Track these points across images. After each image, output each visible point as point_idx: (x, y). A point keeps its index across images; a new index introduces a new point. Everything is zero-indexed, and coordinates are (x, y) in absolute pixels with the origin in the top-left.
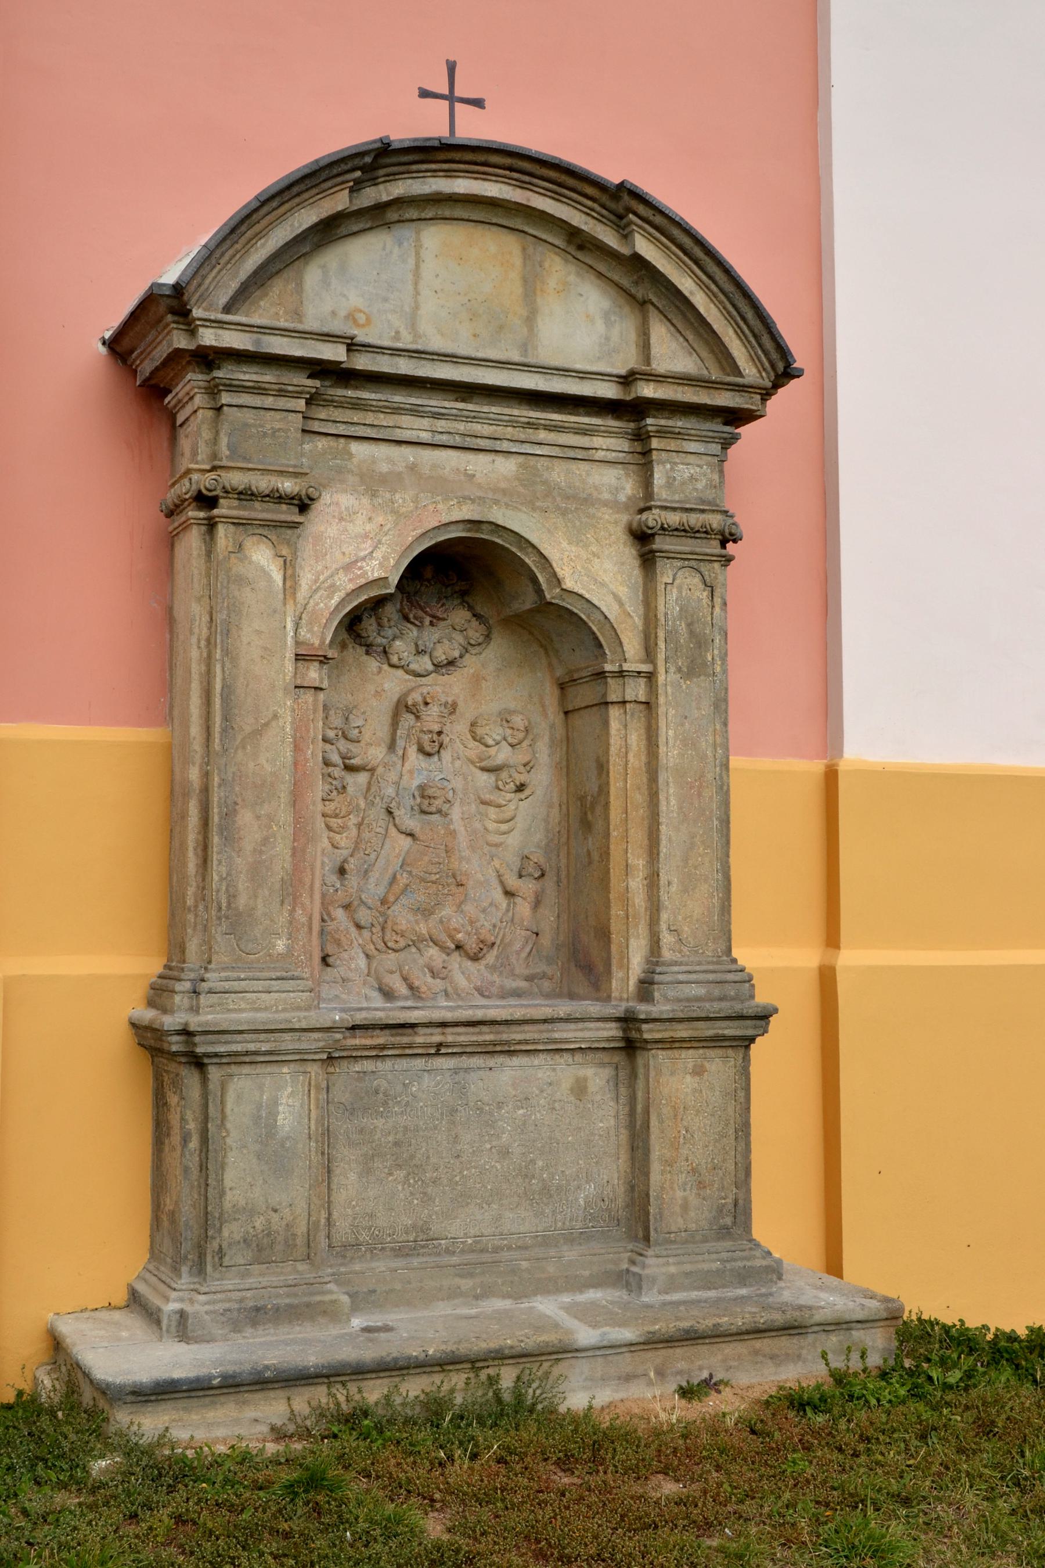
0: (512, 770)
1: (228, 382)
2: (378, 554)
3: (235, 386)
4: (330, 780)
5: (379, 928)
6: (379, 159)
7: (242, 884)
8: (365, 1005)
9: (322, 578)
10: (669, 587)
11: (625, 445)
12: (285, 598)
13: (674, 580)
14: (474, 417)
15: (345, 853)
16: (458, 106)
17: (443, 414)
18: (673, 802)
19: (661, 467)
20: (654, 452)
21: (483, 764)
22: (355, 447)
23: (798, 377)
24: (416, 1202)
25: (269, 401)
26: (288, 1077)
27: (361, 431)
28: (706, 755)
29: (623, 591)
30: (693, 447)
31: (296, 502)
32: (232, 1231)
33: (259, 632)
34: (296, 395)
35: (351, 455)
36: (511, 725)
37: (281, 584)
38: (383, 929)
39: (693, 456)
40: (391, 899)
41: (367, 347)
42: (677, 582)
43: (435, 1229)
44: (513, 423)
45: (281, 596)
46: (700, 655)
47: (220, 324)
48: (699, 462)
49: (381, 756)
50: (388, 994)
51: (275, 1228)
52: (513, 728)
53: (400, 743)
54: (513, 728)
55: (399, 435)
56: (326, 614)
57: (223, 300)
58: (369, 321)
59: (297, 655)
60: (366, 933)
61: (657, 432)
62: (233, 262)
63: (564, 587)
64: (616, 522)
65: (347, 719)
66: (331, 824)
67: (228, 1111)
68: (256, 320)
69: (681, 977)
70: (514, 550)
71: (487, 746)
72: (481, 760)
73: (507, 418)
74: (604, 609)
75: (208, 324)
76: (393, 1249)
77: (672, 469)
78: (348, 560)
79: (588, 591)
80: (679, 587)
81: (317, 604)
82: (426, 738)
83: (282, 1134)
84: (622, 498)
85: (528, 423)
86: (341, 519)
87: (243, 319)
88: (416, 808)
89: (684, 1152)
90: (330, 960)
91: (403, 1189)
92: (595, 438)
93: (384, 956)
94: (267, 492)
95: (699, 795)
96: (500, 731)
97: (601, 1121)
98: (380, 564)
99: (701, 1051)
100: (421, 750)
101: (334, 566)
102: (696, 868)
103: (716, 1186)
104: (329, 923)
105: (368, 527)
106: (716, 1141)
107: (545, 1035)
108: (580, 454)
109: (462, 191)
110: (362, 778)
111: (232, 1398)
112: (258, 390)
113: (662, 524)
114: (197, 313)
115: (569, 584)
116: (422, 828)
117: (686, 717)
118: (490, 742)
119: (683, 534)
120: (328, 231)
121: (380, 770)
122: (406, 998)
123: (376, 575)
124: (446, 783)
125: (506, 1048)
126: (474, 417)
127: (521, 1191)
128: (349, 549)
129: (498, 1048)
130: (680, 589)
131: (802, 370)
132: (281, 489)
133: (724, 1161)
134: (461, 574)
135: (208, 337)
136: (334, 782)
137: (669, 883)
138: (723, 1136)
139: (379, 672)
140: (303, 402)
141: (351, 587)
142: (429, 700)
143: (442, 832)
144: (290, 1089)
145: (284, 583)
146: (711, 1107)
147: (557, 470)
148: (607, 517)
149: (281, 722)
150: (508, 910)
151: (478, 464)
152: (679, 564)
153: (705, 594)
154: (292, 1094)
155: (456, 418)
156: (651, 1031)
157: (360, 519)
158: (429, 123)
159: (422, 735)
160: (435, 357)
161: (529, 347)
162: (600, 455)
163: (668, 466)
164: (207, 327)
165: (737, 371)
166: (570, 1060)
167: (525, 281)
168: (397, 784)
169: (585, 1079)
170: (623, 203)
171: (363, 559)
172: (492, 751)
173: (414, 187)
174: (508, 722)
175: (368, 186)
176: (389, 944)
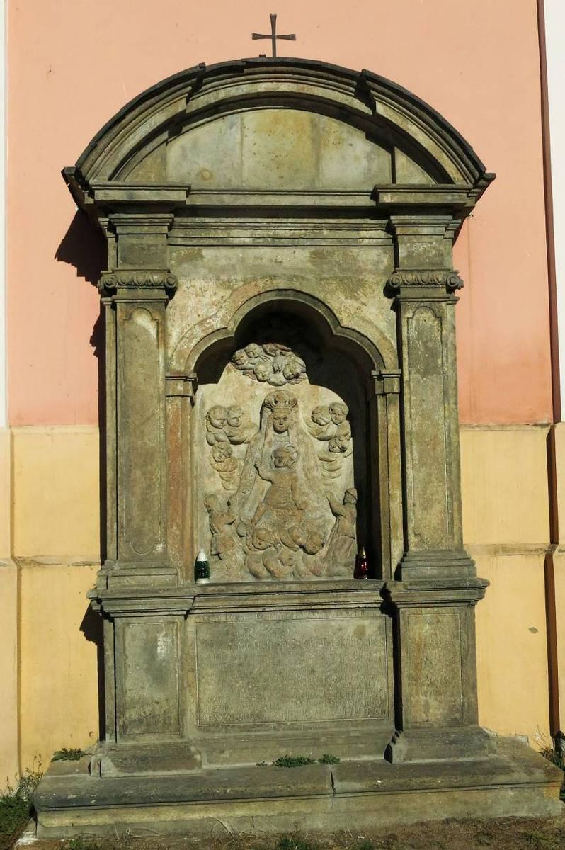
0: (337, 439)
1: (118, 220)
2: (220, 314)
3: (123, 222)
4: (220, 450)
5: (250, 536)
6: (197, 78)
7: (135, 512)
8: (240, 581)
9: (185, 331)
10: (410, 320)
11: (383, 234)
12: (158, 345)
13: (413, 316)
14: (279, 227)
15: (232, 492)
16: (278, 41)
17: (259, 227)
18: (415, 454)
19: (403, 246)
20: (399, 236)
21: (319, 436)
22: (205, 252)
23: (494, 179)
24: (253, 699)
25: (146, 229)
26: (163, 625)
27: (208, 242)
28: (438, 424)
29: (383, 325)
30: (425, 231)
31: (163, 287)
32: (132, 714)
33: (142, 366)
34: (162, 224)
35: (202, 257)
37: (155, 337)
38: (253, 536)
39: (426, 237)
40: (257, 519)
41: (201, 191)
42: (416, 316)
43: (269, 714)
44: (304, 228)
45: (155, 343)
46: (435, 360)
47: (105, 187)
48: (430, 240)
49: (253, 434)
50: (255, 575)
51: (157, 713)
53: (264, 426)
55: (237, 241)
56: (188, 352)
57: (109, 172)
58: (211, 175)
59: (166, 377)
60: (244, 539)
61: (399, 224)
62: (114, 150)
63: (342, 325)
64: (377, 283)
65: (228, 413)
66: (223, 476)
67: (127, 645)
68: (128, 181)
69: (420, 564)
70: (311, 305)
71: (321, 425)
73: (299, 225)
74: (370, 337)
75: (99, 188)
76: (239, 727)
77: (411, 246)
78: (202, 319)
79: (358, 326)
80: (418, 320)
81: (183, 346)
82: (277, 422)
83: (160, 658)
84: (382, 267)
85: (314, 227)
86: (197, 295)
87: (120, 183)
88: (273, 464)
89: (425, 672)
90: (221, 555)
91: (245, 692)
92: (361, 232)
93: (254, 553)
94: (143, 282)
95: (434, 449)
96: (329, 416)
97: (376, 653)
98: (221, 319)
99: (436, 609)
100: (275, 430)
101: (193, 323)
102: (432, 495)
103: (448, 694)
104: (220, 534)
105: (214, 298)
106: (447, 665)
107: (333, 600)
108: (352, 242)
109: (262, 90)
110: (243, 447)
111: (107, 811)
112: (137, 223)
113: (403, 281)
114: (92, 182)
115: (345, 323)
117: (423, 401)
118: (323, 423)
119: (419, 286)
120: (176, 126)
121: (252, 442)
122: (268, 578)
123: (219, 327)
125: (309, 607)
126: (279, 227)
127: (322, 694)
128: (203, 312)
129: (304, 608)
130: (418, 320)
131: (495, 174)
132: (152, 281)
133: (453, 678)
134: (284, 322)
135: (101, 195)
136: (222, 451)
137: (414, 505)
138: (452, 662)
140: (166, 228)
141: (204, 335)
142: (277, 400)
144: (164, 632)
145: (158, 336)
146: (443, 644)
147: (337, 253)
148: (371, 280)
149: (157, 417)
150: (336, 524)
151: (284, 254)
152: (417, 305)
153: (436, 323)
154: (166, 635)
155: (267, 228)
156: (112, 605)
157: (208, 294)
158: (263, 49)
159: (274, 421)
160: (247, 193)
161: (316, 180)
162: (366, 242)
163: (409, 245)
164: (99, 189)
165: (449, 180)
166: (353, 615)
167: (313, 140)
168: (261, 450)
169: (364, 627)
170: (365, 84)
171: (211, 317)
172: (324, 428)
173: (232, 92)
174: (332, 410)
175: (193, 96)
176: (256, 546)
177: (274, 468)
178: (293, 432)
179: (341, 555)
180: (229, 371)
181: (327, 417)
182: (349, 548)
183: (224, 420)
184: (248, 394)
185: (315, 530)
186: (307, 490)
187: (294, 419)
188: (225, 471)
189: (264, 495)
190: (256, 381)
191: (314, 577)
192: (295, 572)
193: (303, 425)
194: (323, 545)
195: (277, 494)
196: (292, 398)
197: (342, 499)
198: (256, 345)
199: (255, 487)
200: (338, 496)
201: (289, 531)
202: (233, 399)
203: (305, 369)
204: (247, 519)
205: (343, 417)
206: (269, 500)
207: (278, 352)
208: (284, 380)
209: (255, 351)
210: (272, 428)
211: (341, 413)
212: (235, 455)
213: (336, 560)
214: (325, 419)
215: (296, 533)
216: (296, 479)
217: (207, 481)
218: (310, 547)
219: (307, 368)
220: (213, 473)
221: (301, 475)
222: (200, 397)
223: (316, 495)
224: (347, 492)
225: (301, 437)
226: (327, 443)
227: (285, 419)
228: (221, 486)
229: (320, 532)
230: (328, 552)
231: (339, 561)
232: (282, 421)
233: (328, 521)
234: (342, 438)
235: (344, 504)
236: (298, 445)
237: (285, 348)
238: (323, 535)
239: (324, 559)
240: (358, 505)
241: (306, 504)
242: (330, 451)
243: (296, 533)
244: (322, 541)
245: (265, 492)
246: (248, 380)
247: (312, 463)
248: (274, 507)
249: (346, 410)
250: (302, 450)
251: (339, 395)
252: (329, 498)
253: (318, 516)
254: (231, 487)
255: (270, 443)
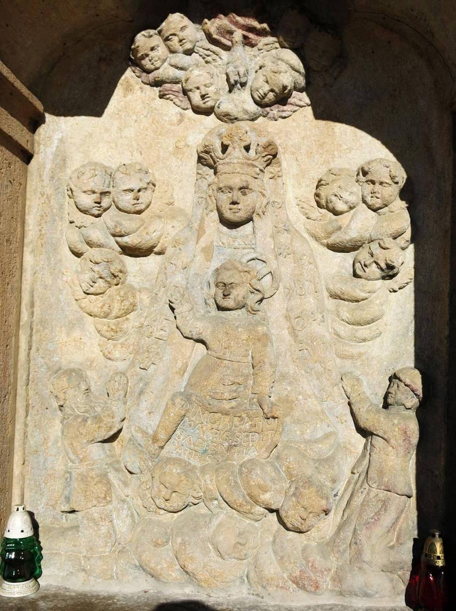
0: (375, 247)
36: (369, 177)
52: (373, 182)
54: (373, 182)
71: (336, 213)
72: (329, 234)
82: (225, 198)
88: (211, 302)
93: (155, 518)
96: (356, 188)
100: (224, 221)
110: (151, 261)
116: (213, 332)
118: (340, 206)
121: (169, 251)
124: (259, 266)
136: (96, 268)
139: (181, 121)
143: (244, 337)
150: (363, 455)
172: (343, 220)
177: (214, 312)
178: (264, 225)
179: (374, 541)
180: (129, 89)
181: (352, 192)
182: (394, 524)
183: (104, 194)
184: (169, 143)
185: (309, 471)
186: (291, 369)
187: (267, 193)
188: (106, 316)
189: (186, 376)
190: (190, 113)
191: (301, 593)
192: (252, 575)
193: (294, 214)
194: (326, 512)
195: (216, 376)
196: (263, 141)
197: (382, 393)
198: (186, 21)
199: (167, 357)
200: (372, 388)
201: (241, 473)
202: (136, 154)
203: (302, 81)
204: (144, 433)
205: (391, 191)
206: (195, 400)
207: (238, 34)
208: (253, 108)
209: (182, 34)
210: (215, 215)
211: (389, 181)
212: (133, 279)
213: (359, 553)
214: (346, 196)
215: (257, 478)
216: (264, 339)
217: (62, 336)
218: (292, 519)
219: (307, 77)
220: (80, 320)
221: (279, 331)
222: (56, 142)
223: (316, 382)
224: (394, 378)
225: (284, 238)
226: (349, 257)
227: (244, 189)
228: (97, 350)
229: (322, 478)
230: (340, 528)
231: (367, 556)
232: (237, 195)
233: (344, 448)
234: (388, 242)
235: (386, 406)
236: (276, 257)
237: (255, 24)
238: (329, 484)
239: (331, 545)
240: (423, 412)
241: (289, 403)
242: (355, 275)
243: (257, 478)
244: (324, 502)
245: (190, 369)
246: (171, 110)
247: (310, 302)
248: (208, 409)
249: (402, 175)
250: (286, 269)
251: (385, 143)
252: (349, 390)
253: (320, 434)
254: (117, 354)
255: (208, 252)
